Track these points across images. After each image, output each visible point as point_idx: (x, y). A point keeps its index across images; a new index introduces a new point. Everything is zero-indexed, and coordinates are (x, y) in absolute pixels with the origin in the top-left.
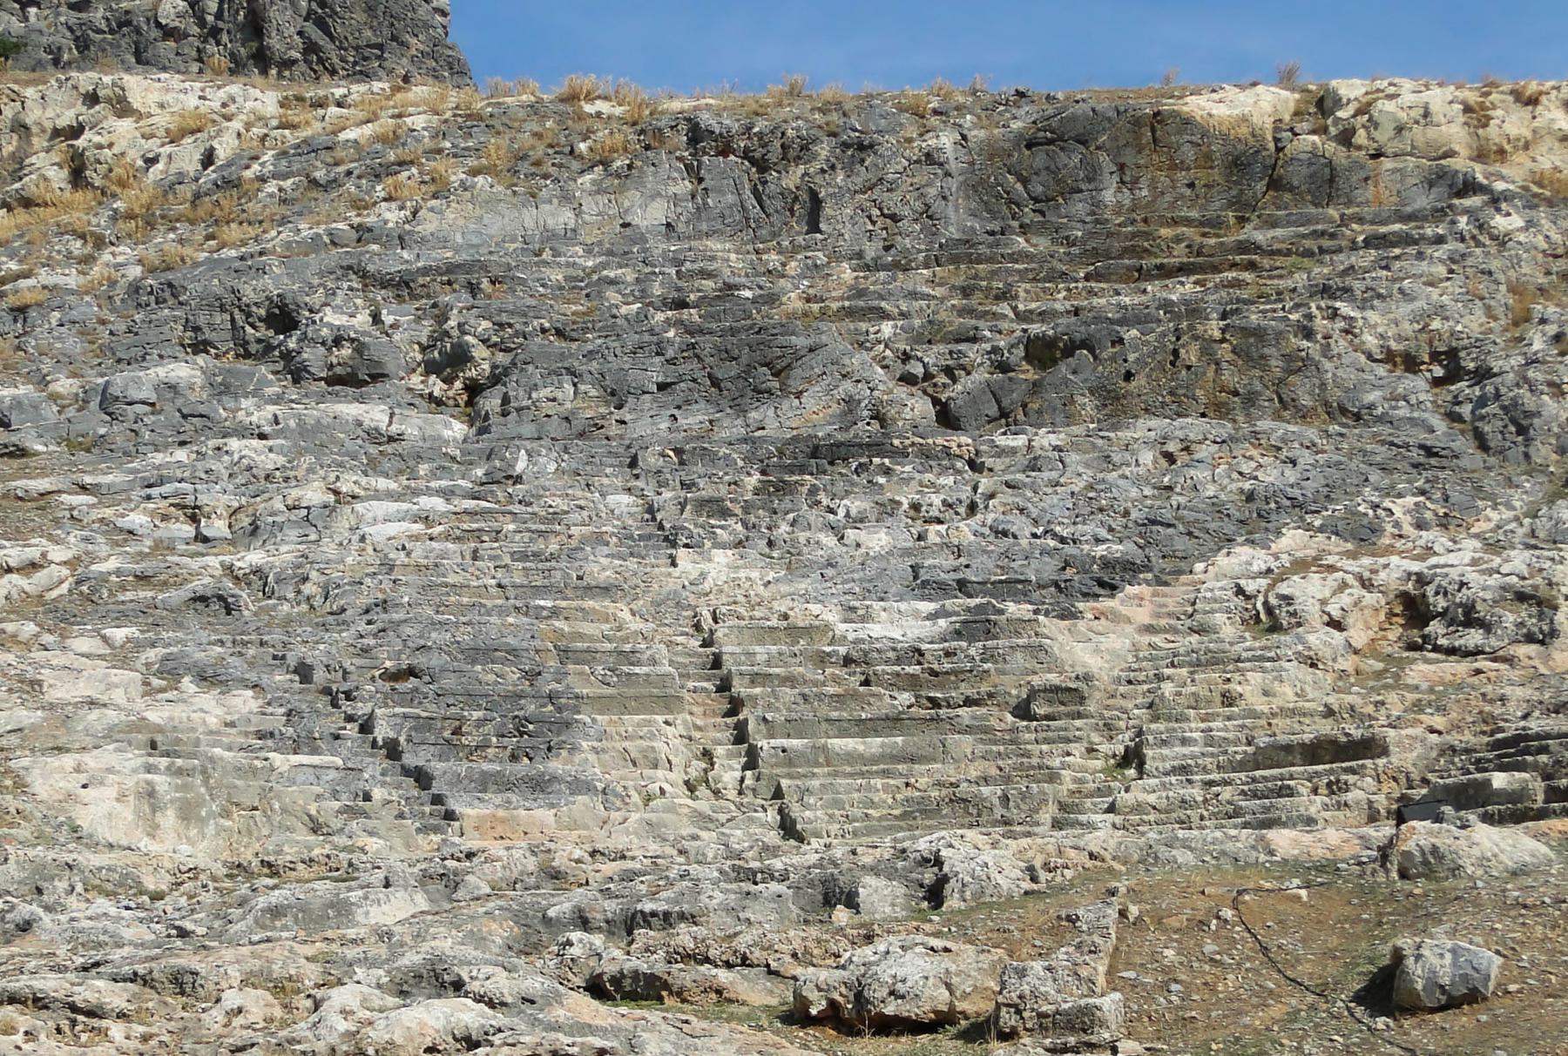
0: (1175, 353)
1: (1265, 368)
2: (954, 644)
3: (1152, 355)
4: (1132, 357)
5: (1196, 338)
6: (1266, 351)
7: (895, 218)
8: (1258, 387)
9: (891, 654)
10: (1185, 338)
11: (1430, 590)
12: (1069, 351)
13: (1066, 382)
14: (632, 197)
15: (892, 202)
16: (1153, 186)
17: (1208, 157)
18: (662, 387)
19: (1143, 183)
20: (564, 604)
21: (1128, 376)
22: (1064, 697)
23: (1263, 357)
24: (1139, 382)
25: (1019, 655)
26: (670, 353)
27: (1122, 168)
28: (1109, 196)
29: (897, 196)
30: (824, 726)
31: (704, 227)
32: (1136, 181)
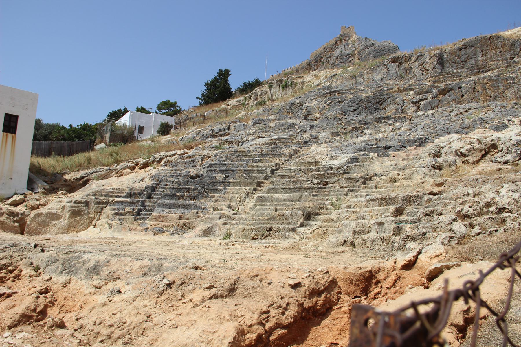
0: (475, 88)
1: (499, 89)
2: (350, 165)
3: (469, 89)
4: (463, 91)
5: (480, 84)
6: (499, 84)
7: (427, 70)
8: (497, 94)
9: (325, 169)
10: (477, 84)
11: (500, 143)
12: (448, 91)
13: (447, 99)
14: (374, 74)
15: (426, 66)
16: (491, 54)
17: (505, 44)
18: (355, 110)
19: (488, 53)
20: (262, 158)
21: (462, 96)
22: (351, 180)
23: (498, 86)
24: (465, 97)
25: (357, 168)
26: (357, 102)
27: (482, 51)
28: (480, 58)
29: (428, 65)
30: (281, 190)
31: (389, 78)
32: (486, 53)
